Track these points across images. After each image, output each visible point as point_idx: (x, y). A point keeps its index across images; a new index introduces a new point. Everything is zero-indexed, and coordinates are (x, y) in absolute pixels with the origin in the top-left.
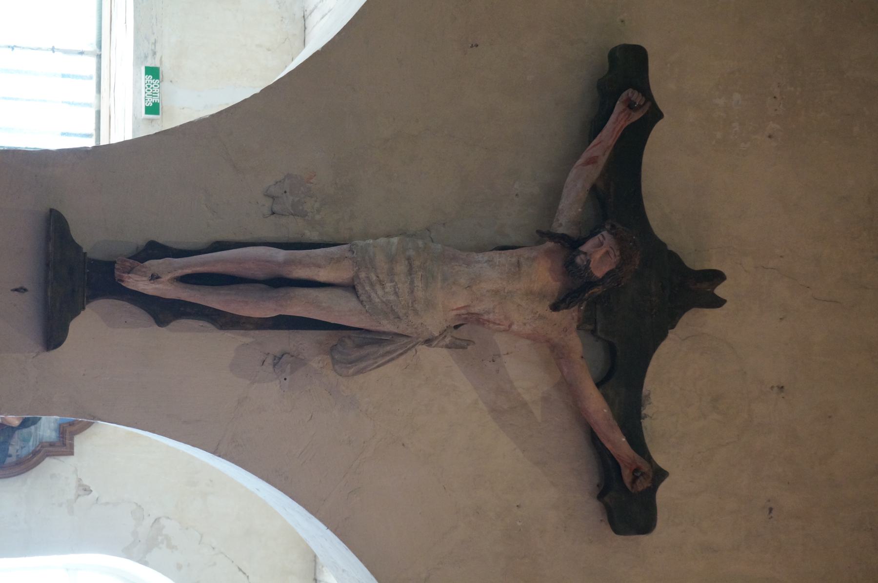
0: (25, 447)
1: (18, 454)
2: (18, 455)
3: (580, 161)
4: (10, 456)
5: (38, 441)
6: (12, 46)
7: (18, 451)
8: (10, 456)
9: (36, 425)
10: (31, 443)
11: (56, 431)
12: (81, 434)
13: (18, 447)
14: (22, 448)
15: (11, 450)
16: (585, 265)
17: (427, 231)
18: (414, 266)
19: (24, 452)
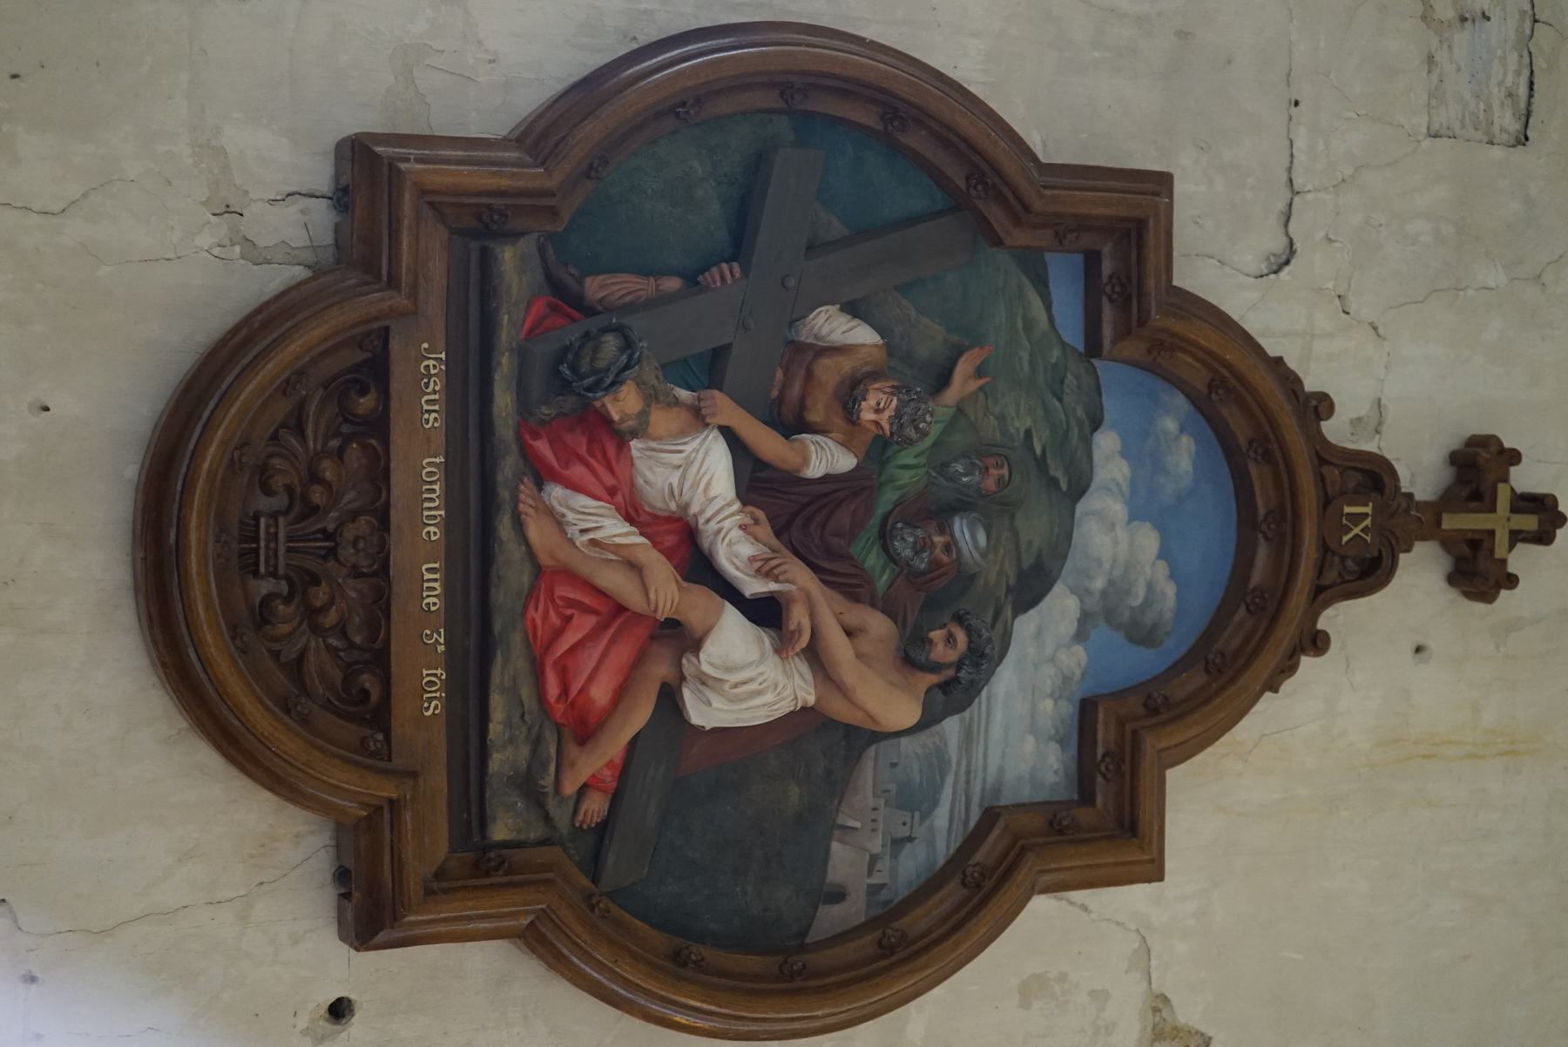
0: (910, 839)
1: (874, 880)
2: (874, 890)
3: (614, 463)
4: (838, 895)
5: (976, 799)
6: (1289, 195)
7: (878, 866)
8: (838, 895)
9: (967, 714)
10: (941, 817)
11: (1062, 742)
12: (233, 772)
13: (876, 845)
14: (898, 844)
15: (843, 863)
16: (1055, 366)
17: (492, 58)
18: (708, 534)
19: (911, 865)
